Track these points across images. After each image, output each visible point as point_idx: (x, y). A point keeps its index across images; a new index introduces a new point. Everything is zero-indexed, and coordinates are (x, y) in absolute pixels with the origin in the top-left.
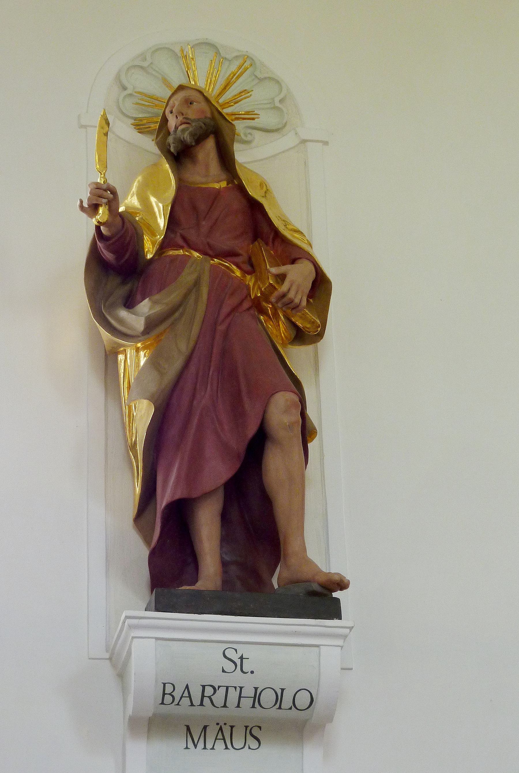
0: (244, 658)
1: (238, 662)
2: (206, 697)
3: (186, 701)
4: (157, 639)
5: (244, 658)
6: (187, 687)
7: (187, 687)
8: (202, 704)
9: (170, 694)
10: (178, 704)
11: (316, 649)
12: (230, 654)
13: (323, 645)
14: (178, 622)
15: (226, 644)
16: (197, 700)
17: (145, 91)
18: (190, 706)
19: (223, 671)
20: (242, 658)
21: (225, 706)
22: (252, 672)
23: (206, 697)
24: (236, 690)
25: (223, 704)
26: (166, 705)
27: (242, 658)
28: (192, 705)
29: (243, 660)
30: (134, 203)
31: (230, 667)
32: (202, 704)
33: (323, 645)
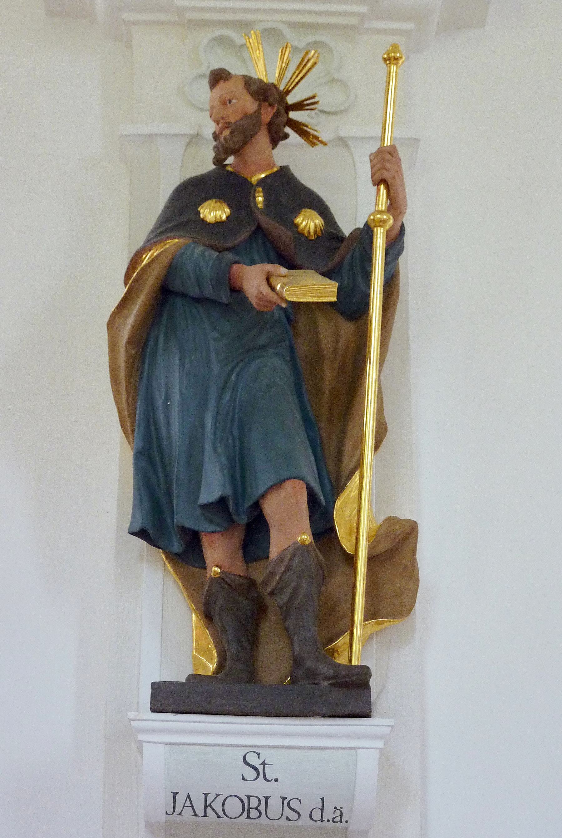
0: (267, 764)
1: (261, 768)
2: (253, 808)
3: (188, 812)
4: (167, 744)
5: (267, 764)
6: (188, 796)
7: (188, 796)
8: (205, 815)
9: (256, 809)
10: (180, 814)
11: (353, 751)
12: (252, 759)
13: (359, 748)
14: (238, 726)
15: (248, 748)
16: (200, 811)
17: (376, 194)
18: (193, 816)
19: (243, 779)
20: (264, 764)
21: (322, 820)
22: (276, 780)
23: (253, 808)
24: (300, 803)
25: (204, 814)
26: (292, 821)
27: (264, 764)
28: (195, 815)
29: (266, 765)
30: (221, 217)
31: (250, 774)
32: (205, 815)
33: (359, 748)
